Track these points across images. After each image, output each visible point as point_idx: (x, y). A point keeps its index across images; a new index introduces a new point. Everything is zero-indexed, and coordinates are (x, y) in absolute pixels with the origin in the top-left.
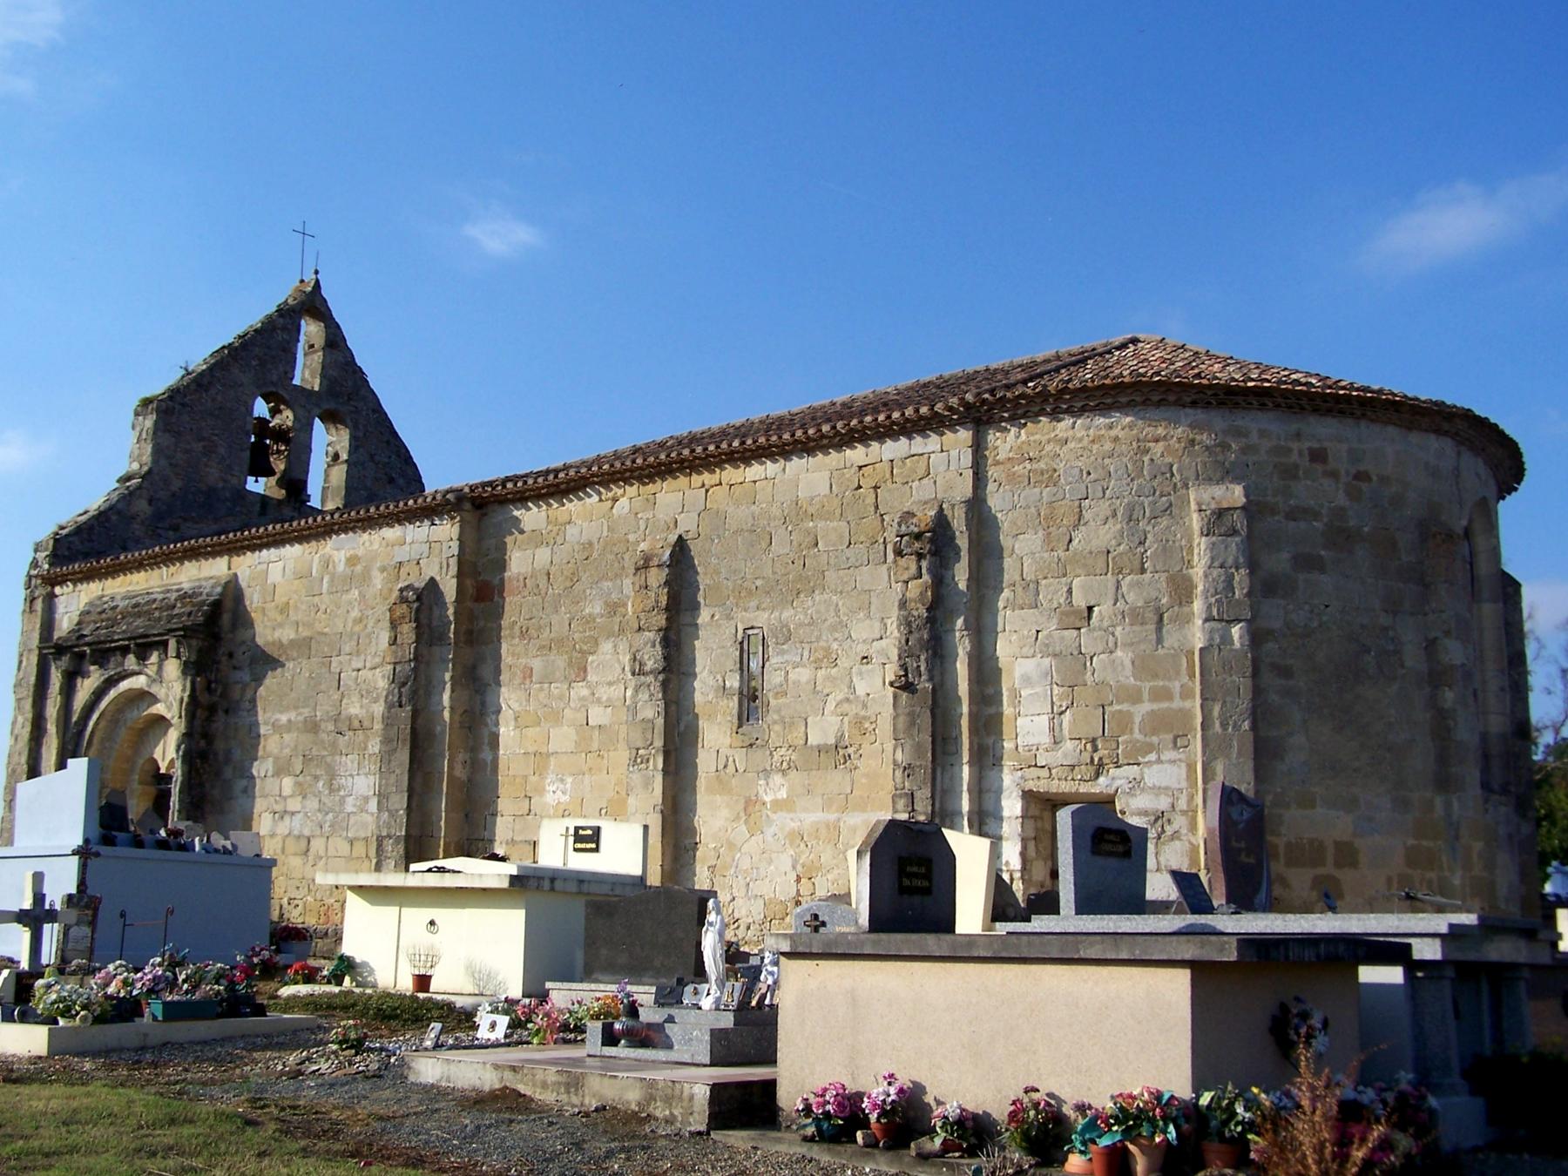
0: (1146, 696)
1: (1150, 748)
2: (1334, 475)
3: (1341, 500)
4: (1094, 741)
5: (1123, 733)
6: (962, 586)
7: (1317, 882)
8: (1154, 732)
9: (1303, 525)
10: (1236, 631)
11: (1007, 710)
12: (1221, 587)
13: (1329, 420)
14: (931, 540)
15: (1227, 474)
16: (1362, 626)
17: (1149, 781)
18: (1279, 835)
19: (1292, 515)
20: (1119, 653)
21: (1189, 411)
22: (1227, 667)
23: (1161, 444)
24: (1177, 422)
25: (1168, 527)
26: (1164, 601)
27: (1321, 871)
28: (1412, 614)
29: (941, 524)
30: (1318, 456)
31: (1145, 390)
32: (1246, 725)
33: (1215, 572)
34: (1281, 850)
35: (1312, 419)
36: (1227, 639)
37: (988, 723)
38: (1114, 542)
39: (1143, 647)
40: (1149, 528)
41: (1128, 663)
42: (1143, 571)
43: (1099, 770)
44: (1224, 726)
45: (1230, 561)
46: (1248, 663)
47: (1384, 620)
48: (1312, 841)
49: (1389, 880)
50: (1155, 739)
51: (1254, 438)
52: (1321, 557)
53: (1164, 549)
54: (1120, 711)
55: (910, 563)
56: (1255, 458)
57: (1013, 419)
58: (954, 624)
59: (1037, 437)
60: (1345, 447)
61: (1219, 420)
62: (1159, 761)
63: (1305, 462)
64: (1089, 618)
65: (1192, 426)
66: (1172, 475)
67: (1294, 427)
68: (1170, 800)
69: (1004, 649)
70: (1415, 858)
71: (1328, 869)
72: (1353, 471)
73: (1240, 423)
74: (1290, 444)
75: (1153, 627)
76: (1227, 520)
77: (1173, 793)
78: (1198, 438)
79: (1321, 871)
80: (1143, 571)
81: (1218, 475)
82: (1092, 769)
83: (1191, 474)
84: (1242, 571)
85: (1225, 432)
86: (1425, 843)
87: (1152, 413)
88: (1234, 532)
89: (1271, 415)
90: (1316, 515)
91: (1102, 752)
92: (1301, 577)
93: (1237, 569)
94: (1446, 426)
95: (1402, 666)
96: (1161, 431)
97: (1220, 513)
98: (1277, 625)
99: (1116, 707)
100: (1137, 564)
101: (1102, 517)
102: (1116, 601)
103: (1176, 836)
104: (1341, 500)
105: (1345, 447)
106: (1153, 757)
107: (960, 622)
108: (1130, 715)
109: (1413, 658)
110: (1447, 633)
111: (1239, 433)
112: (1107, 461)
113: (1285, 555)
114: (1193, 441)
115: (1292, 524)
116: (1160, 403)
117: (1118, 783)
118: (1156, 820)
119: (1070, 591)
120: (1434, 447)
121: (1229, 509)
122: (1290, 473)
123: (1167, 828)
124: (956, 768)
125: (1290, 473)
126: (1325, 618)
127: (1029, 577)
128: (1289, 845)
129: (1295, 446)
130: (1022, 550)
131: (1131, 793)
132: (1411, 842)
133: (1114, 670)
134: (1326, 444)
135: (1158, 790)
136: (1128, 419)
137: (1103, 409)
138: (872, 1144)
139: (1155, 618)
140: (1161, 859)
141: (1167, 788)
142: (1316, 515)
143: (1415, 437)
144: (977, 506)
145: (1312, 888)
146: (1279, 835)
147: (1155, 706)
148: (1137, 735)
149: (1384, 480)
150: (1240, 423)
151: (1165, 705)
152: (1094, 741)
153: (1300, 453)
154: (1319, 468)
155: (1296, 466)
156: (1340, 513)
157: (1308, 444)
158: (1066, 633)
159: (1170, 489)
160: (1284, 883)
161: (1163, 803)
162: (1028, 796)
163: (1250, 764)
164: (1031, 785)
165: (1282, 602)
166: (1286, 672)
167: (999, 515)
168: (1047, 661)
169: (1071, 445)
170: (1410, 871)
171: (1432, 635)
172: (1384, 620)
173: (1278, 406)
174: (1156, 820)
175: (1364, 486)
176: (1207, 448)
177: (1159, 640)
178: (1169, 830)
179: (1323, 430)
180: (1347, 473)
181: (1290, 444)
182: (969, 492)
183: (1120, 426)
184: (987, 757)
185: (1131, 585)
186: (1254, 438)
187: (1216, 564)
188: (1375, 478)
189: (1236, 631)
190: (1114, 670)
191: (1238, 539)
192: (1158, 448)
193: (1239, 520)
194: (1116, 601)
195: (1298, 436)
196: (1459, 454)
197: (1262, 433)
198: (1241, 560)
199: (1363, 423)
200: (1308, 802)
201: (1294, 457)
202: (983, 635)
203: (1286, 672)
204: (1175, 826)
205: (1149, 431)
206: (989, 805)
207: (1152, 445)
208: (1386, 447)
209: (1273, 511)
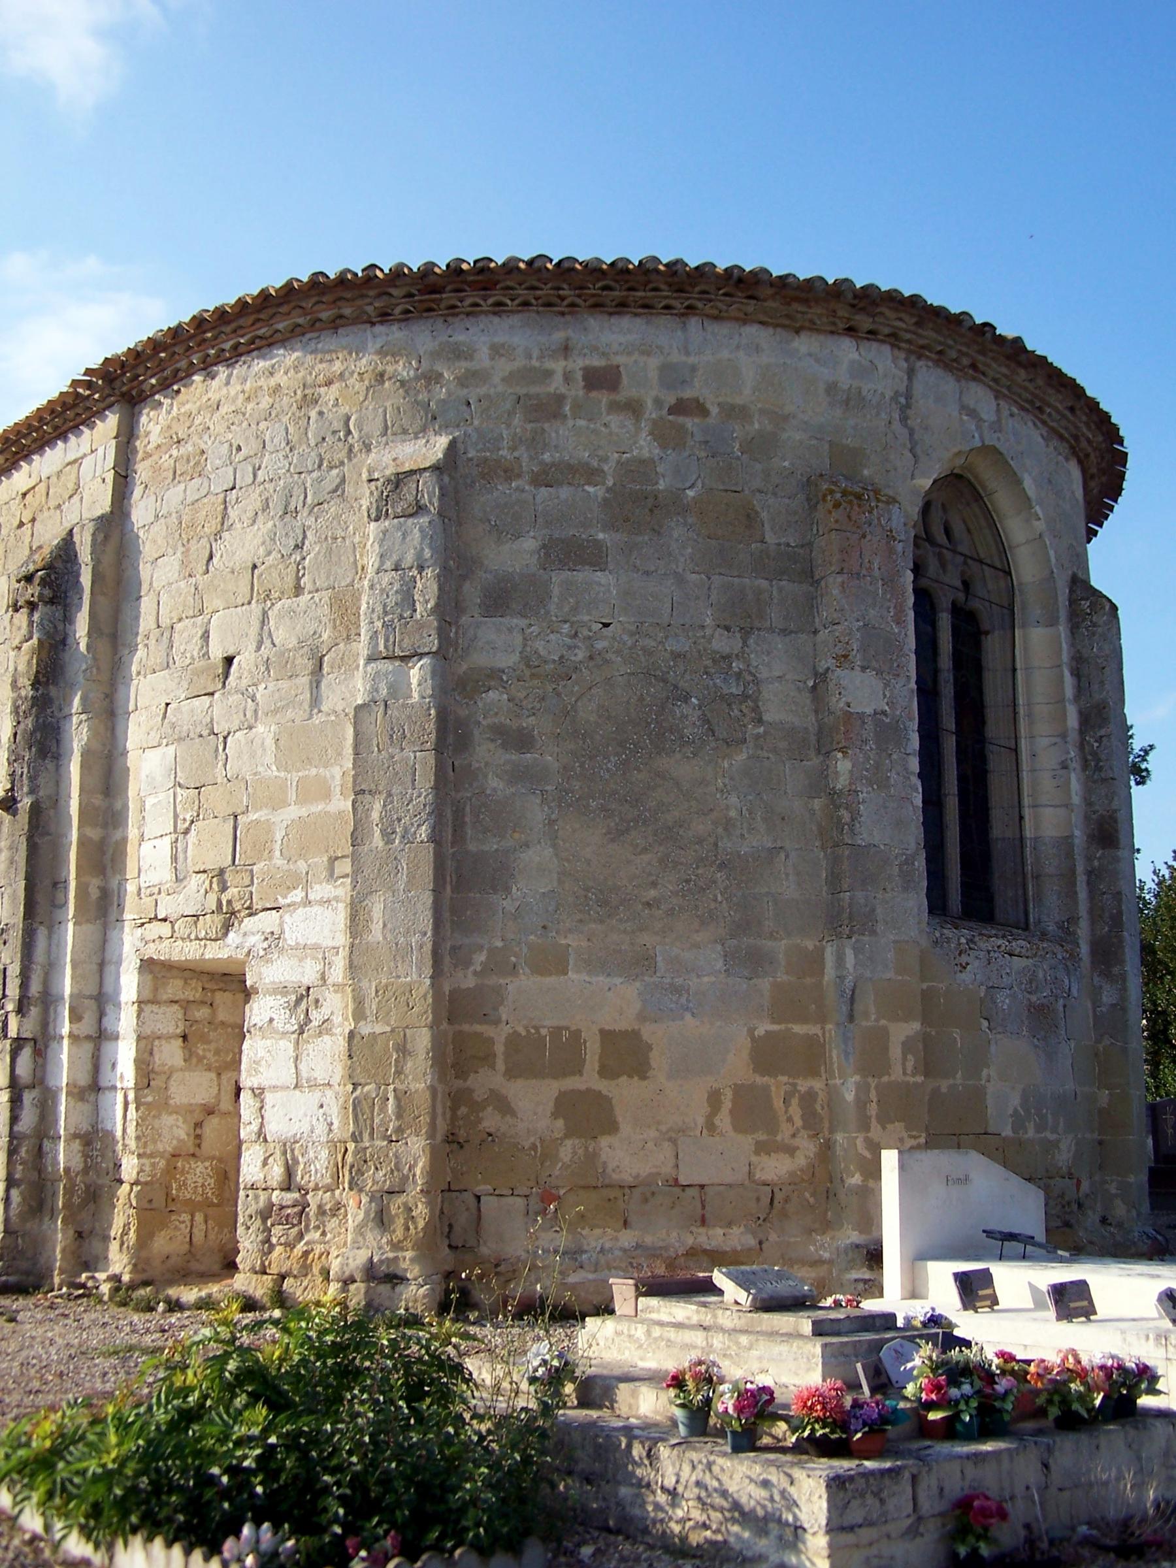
0: (292, 795)
1: (294, 881)
2: (633, 408)
3: (645, 446)
4: (222, 872)
5: (260, 859)
6: (83, 647)
7: (565, 1105)
8: (303, 854)
9: (565, 492)
10: (416, 673)
11: (132, 833)
12: (392, 601)
13: (625, 322)
14: (44, 583)
15: (432, 419)
16: (676, 656)
17: (290, 938)
18: (497, 1022)
19: (544, 478)
20: (260, 728)
21: (379, 329)
22: (396, 736)
23: (335, 387)
24: (360, 350)
25: (337, 517)
26: (325, 636)
27: (573, 1083)
28: (785, 632)
29: (66, 550)
30: (602, 379)
31: (308, 304)
32: (423, 832)
33: (386, 578)
34: (499, 1049)
35: (594, 322)
36: (398, 689)
37: (106, 857)
38: (261, 551)
39: (290, 714)
40: (310, 521)
41: (270, 742)
42: (298, 590)
43: (229, 919)
44: (388, 836)
45: (409, 559)
46: (431, 726)
47: (722, 643)
48: (556, 1031)
49: (714, 1099)
50: (302, 866)
51: (483, 358)
52: (597, 544)
53: (330, 551)
54: (257, 822)
55: (22, 617)
56: (482, 390)
57: (164, 386)
58: (70, 704)
59: (188, 407)
60: (654, 363)
61: (424, 337)
62: (307, 902)
63: (577, 390)
64: (226, 675)
65: (382, 352)
66: (349, 432)
67: (559, 336)
68: (319, 967)
69: (137, 732)
70: (768, 1056)
71: (590, 1079)
72: (671, 400)
73: (460, 337)
74: (549, 365)
75: (304, 680)
76: (408, 491)
77: (324, 955)
78: (390, 369)
79: (573, 1083)
80: (298, 590)
81: (419, 423)
82: (218, 919)
83: (375, 427)
84: (429, 572)
85: (435, 355)
86: (798, 1029)
87: (329, 341)
88: (419, 509)
89: (515, 320)
90: (592, 475)
91: (232, 892)
92: (558, 578)
93: (421, 569)
94: (864, 322)
95: (760, 721)
96: (337, 367)
97: (398, 481)
98: (507, 661)
99: (253, 816)
100: (290, 581)
101: (251, 514)
102: (260, 644)
103: (325, 1027)
104: (645, 446)
105: (654, 363)
106: (297, 895)
107: (77, 701)
108: (268, 827)
109: (782, 703)
110: (843, 659)
111: (458, 353)
112: (263, 425)
113: (529, 544)
114: (382, 375)
115: (544, 492)
116: (336, 324)
117: (252, 940)
118: (298, 1001)
119: (206, 636)
120: (875, 367)
121: (412, 472)
122: (547, 409)
123: (314, 1014)
124: (63, 925)
125: (547, 409)
126: (600, 645)
127: (165, 621)
128: (513, 1041)
129: (558, 366)
130: (161, 576)
131: (265, 958)
132: (764, 1027)
133: (253, 756)
134: (620, 360)
135: (304, 950)
136: (296, 355)
137: (262, 345)
138: (24, 1532)
139: (310, 665)
140: (303, 1067)
141: (316, 947)
142: (592, 475)
143: (804, 344)
144: (114, 526)
145: (555, 1115)
146: (497, 1022)
147: (304, 812)
148: (278, 861)
149: (734, 412)
150: (460, 337)
151: (318, 807)
152: (222, 872)
153: (568, 377)
154: (603, 398)
155: (560, 399)
156: (641, 469)
157: (581, 363)
158: (196, 702)
159: (343, 455)
160: (504, 1107)
161: (308, 973)
162: (148, 966)
163: (427, 898)
164: (151, 952)
165: (523, 623)
166: (522, 741)
167: (141, 534)
168: (172, 748)
169: (224, 410)
170: (760, 1080)
171: (822, 666)
172: (722, 643)
173: (526, 304)
174: (298, 1001)
175: (690, 423)
176: (403, 383)
177: (315, 702)
178: (316, 1016)
179: (614, 337)
180: (658, 402)
181: (549, 365)
182: (104, 504)
183: (280, 371)
184: (104, 908)
185: (280, 616)
186: (483, 358)
187: (388, 565)
188: (714, 410)
189: (416, 673)
190: (253, 756)
191: (424, 520)
192: (330, 394)
193: (428, 489)
194: (260, 644)
195: (566, 350)
196: (911, 373)
197: (497, 351)
198: (427, 553)
199: (694, 322)
200: (552, 962)
201: (556, 384)
202: (110, 715)
203: (522, 741)
204: (325, 1011)
205: (322, 369)
206: (108, 988)
207: (323, 390)
208: (737, 359)
209: (510, 473)
